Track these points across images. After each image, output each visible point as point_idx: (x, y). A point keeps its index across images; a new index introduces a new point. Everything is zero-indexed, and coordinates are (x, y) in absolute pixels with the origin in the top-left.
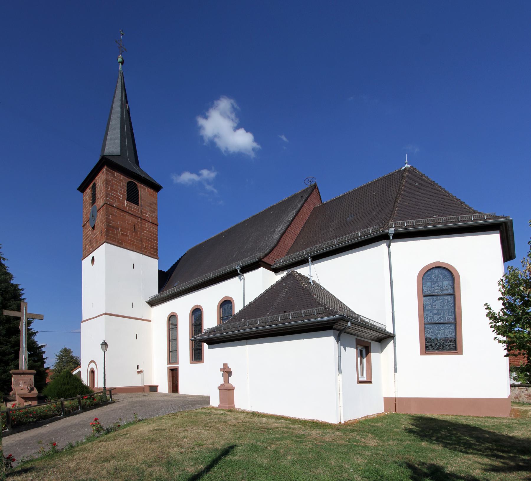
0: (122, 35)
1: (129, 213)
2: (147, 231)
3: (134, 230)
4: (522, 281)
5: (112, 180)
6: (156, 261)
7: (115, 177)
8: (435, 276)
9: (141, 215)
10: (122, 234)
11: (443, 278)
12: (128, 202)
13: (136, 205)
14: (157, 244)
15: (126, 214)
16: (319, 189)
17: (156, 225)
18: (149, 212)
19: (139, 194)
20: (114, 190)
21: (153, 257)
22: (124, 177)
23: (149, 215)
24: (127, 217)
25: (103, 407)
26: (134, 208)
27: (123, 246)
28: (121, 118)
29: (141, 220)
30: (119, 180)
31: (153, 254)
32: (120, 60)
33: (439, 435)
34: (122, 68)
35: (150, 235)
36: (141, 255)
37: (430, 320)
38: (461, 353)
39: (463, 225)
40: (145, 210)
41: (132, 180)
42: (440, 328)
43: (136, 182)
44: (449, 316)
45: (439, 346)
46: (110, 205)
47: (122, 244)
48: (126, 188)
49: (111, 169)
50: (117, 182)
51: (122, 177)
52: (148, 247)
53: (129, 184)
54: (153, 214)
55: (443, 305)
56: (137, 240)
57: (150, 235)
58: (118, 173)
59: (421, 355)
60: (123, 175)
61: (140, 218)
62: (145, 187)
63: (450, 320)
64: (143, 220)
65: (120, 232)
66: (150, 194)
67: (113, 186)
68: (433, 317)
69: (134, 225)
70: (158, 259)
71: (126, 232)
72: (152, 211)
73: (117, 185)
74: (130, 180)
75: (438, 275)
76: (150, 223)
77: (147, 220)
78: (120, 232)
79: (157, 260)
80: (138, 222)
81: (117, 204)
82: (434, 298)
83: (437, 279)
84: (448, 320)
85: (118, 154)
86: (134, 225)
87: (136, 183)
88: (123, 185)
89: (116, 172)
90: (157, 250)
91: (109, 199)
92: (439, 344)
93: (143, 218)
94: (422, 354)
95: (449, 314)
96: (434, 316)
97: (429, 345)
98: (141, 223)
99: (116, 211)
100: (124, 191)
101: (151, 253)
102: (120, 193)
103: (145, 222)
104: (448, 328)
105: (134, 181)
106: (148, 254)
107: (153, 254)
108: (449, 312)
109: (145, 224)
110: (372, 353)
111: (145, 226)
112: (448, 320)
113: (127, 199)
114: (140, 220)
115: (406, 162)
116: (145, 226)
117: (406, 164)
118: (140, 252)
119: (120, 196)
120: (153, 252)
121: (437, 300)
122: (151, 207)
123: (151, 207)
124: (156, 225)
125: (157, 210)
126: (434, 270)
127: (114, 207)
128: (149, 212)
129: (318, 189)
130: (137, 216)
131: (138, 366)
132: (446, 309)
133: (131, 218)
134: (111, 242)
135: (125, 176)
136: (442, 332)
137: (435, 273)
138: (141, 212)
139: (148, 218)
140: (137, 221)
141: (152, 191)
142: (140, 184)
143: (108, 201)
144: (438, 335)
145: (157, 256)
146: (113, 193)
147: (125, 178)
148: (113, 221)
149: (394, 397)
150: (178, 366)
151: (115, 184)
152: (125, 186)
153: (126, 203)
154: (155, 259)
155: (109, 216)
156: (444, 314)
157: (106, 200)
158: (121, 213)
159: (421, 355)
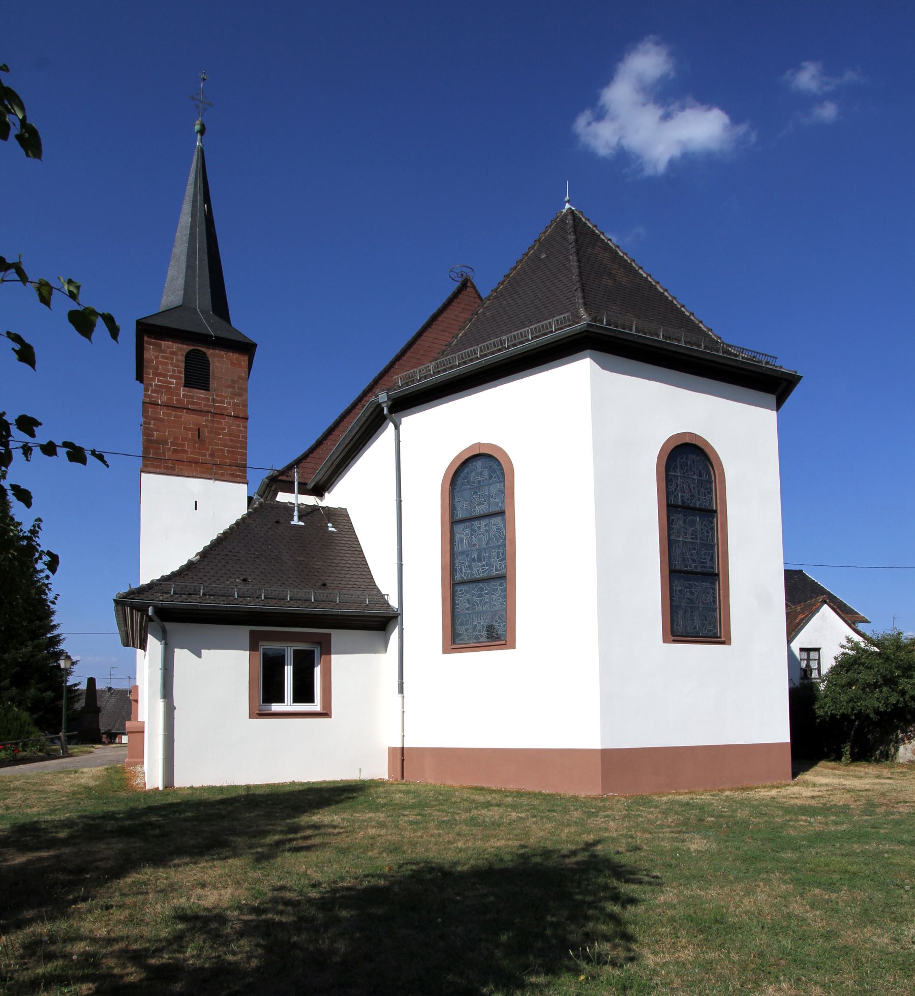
0: (204, 79)
1: (188, 409)
2: (225, 434)
3: (199, 438)
5: (157, 357)
7: (161, 351)
8: (477, 474)
9: (214, 406)
10: (175, 451)
11: (491, 477)
12: (187, 389)
13: (202, 391)
14: (245, 454)
15: (183, 412)
16: (477, 288)
17: (243, 418)
18: (228, 398)
19: (211, 368)
20: (160, 375)
21: (236, 481)
22: (180, 345)
23: (229, 403)
24: (185, 416)
26: (198, 398)
27: (174, 473)
28: (191, 234)
29: (213, 417)
30: (170, 354)
32: (197, 128)
33: (809, 819)
34: (201, 141)
35: (231, 441)
36: (212, 481)
37: (465, 575)
38: (513, 646)
39: (504, 356)
40: (221, 396)
41: (196, 348)
42: (483, 591)
43: (205, 348)
44: (499, 561)
45: (479, 631)
46: (152, 404)
47: (173, 468)
48: (183, 365)
49: (154, 339)
50: (167, 358)
51: (175, 346)
53: (189, 357)
54: (237, 400)
55: (489, 537)
56: (205, 455)
57: (231, 441)
58: (168, 341)
59: (664, 642)
60: (178, 343)
61: (211, 412)
62: (222, 353)
63: (500, 570)
64: (216, 416)
65: (170, 448)
66: (233, 363)
67: (157, 368)
68: (470, 568)
69: (199, 429)
70: (247, 484)
71: (183, 445)
72: (235, 395)
73: (166, 364)
74: (192, 348)
75: (481, 473)
76: (232, 418)
77: (224, 415)
78: (170, 448)
79: (246, 485)
80: (206, 420)
81: (165, 398)
82: (473, 525)
83: (479, 482)
84: (496, 570)
85: (178, 305)
86: (199, 429)
87: (204, 349)
88: (177, 360)
89: (164, 341)
91: (150, 393)
93: (215, 412)
94: (446, 651)
95: (498, 558)
96: (474, 564)
98: (212, 422)
99: (162, 412)
100: (180, 372)
101: (232, 475)
102: (172, 377)
103: (221, 418)
104: (497, 589)
105: (200, 348)
107: (237, 476)
108: (498, 553)
109: (220, 423)
111: (220, 426)
112: (496, 570)
113: (185, 383)
114: (211, 415)
115: (567, 198)
116: (220, 426)
117: (567, 204)
118: (209, 477)
119: (172, 383)
120: (236, 471)
121: (479, 528)
122: (234, 387)
124: (243, 418)
125: (246, 390)
126: (474, 463)
127: (159, 405)
128: (228, 398)
129: (474, 287)
130: (204, 411)
132: (494, 547)
133: (194, 417)
134: (152, 470)
135: (182, 343)
136: (486, 598)
137: (477, 468)
138: (213, 400)
139: (226, 408)
140: (202, 420)
141: (236, 356)
142: (211, 351)
143: (150, 396)
144: (478, 606)
145: (245, 477)
146: (159, 381)
147: (182, 346)
148: (156, 431)
149: (400, 746)
151: (162, 363)
152: (182, 362)
154: (241, 485)
155: (150, 424)
156: (490, 557)
157: (146, 396)
158: (174, 413)
159: (664, 642)
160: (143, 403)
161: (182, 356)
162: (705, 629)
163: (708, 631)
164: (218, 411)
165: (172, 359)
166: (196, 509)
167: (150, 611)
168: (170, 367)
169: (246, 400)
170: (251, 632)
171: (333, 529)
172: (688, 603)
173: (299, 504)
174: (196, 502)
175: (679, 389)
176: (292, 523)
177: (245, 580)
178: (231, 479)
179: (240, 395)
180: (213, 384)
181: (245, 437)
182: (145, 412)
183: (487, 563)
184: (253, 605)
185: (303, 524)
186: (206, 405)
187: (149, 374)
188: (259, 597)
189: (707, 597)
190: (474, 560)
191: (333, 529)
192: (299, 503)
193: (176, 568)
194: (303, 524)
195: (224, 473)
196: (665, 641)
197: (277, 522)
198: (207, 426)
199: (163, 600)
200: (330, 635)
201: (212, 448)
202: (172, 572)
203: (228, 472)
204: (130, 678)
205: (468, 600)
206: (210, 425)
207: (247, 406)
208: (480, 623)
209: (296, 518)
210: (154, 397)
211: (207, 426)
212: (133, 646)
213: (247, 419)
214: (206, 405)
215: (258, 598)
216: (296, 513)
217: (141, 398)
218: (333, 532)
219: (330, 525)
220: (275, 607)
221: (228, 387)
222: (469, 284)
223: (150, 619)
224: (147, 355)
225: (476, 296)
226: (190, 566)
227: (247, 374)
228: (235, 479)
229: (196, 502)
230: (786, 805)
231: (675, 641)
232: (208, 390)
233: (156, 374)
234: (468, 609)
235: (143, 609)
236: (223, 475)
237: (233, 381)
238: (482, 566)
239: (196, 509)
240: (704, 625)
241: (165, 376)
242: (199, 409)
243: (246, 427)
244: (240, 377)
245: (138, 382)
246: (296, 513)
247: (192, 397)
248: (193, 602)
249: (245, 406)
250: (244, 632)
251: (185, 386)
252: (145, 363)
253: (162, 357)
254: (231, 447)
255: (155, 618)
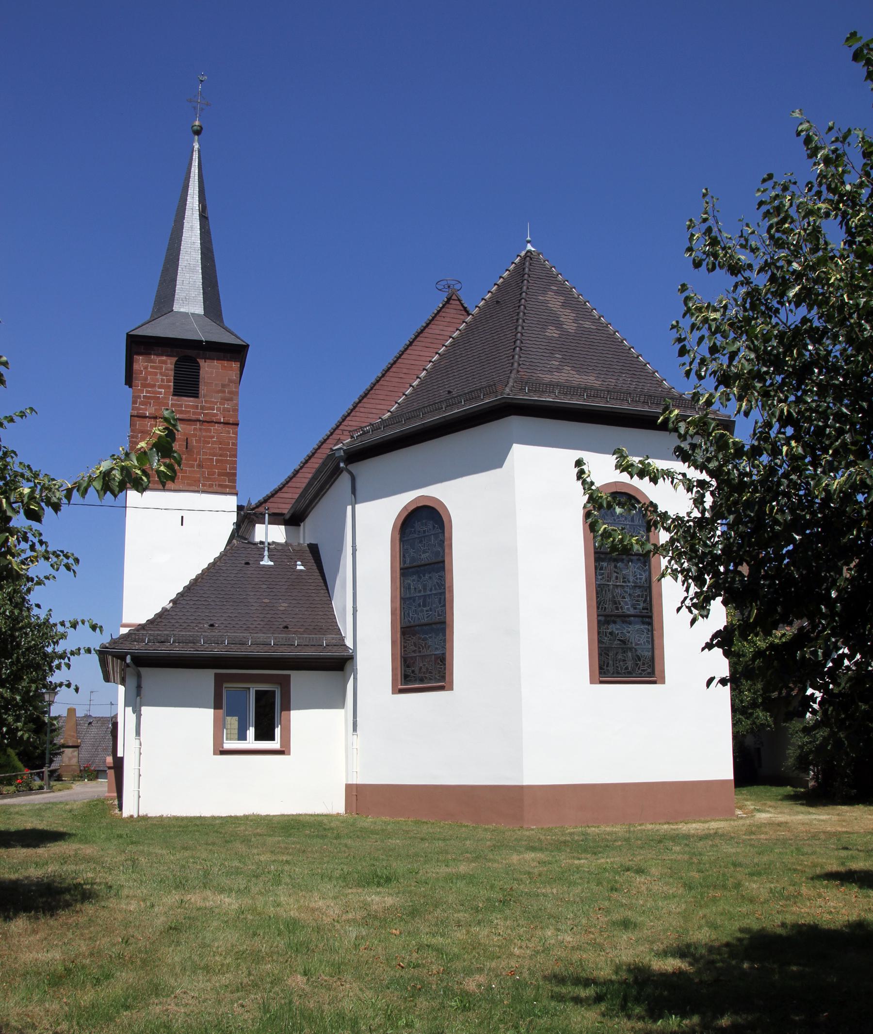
3: (187, 448)
4: (768, 383)
5: (146, 368)
6: (235, 498)
12: (176, 398)
13: (191, 399)
17: (233, 424)
23: (218, 409)
25: (769, 787)
26: (186, 406)
31: (226, 486)
48: (172, 373)
52: (214, 473)
56: (192, 466)
59: (591, 683)
67: (146, 379)
70: (237, 494)
73: (156, 374)
76: (222, 425)
80: (195, 429)
90: (235, 475)
92: (424, 670)
97: (409, 671)
98: (200, 429)
100: (169, 381)
101: (220, 486)
102: (160, 387)
106: (215, 488)
107: (226, 486)
109: (210, 431)
110: (292, 712)
112: (439, 615)
119: (160, 393)
122: (224, 392)
123: (224, 392)
124: (233, 424)
125: (237, 393)
138: (203, 408)
139: (216, 415)
145: (234, 487)
150: (274, 740)
151: (151, 373)
153: (171, 400)
159: (591, 683)
160: (131, 416)
161: (171, 364)
162: (639, 669)
163: (642, 670)
164: (208, 419)
165: (161, 368)
166: (182, 525)
167: (128, 659)
168: (159, 377)
169: (237, 405)
170: (216, 675)
171: (302, 568)
172: (620, 644)
173: (269, 544)
174: (182, 517)
175: (301, 711)
176: (262, 563)
177: (212, 625)
178: (220, 490)
179: (231, 399)
180: (203, 390)
181: (235, 444)
182: (132, 425)
183: (430, 609)
184: (216, 650)
185: (272, 563)
186: (194, 413)
187: (138, 383)
188: (223, 642)
189: (641, 637)
190: (419, 605)
191: (302, 568)
192: (270, 540)
193: (151, 616)
194: (272, 563)
195: (213, 485)
196: (592, 682)
197: (247, 563)
198: (195, 435)
199: (138, 648)
200: (289, 676)
201: (200, 458)
202: (148, 621)
203: (217, 483)
204: (112, 704)
205: (415, 643)
206: (198, 433)
207: (237, 410)
208: (424, 665)
209: (266, 558)
210: (142, 409)
211: (195, 435)
212: (114, 682)
213: (237, 424)
214: (194, 413)
215: (222, 644)
216: (266, 553)
217: (129, 412)
218: (301, 571)
219: (299, 563)
220: (237, 651)
221: (218, 392)
222: (454, 297)
223: (128, 666)
224: (136, 367)
225: (462, 309)
226: (162, 615)
227: (239, 376)
228: (223, 490)
229: (182, 517)
230: (777, 822)
231: (602, 682)
232: (197, 397)
233: (144, 386)
234: (414, 651)
235: (122, 657)
236: (211, 486)
237: (223, 386)
238: (427, 611)
239: (182, 525)
240: (637, 665)
241: (154, 386)
242: (188, 418)
243: (236, 434)
244: (231, 381)
245: (127, 386)
246: (266, 553)
247: (181, 406)
248: (163, 650)
249: (236, 410)
250: (206, 678)
251: (174, 395)
252: (134, 375)
253: (151, 367)
254: (220, 456)
255: (132, 665)
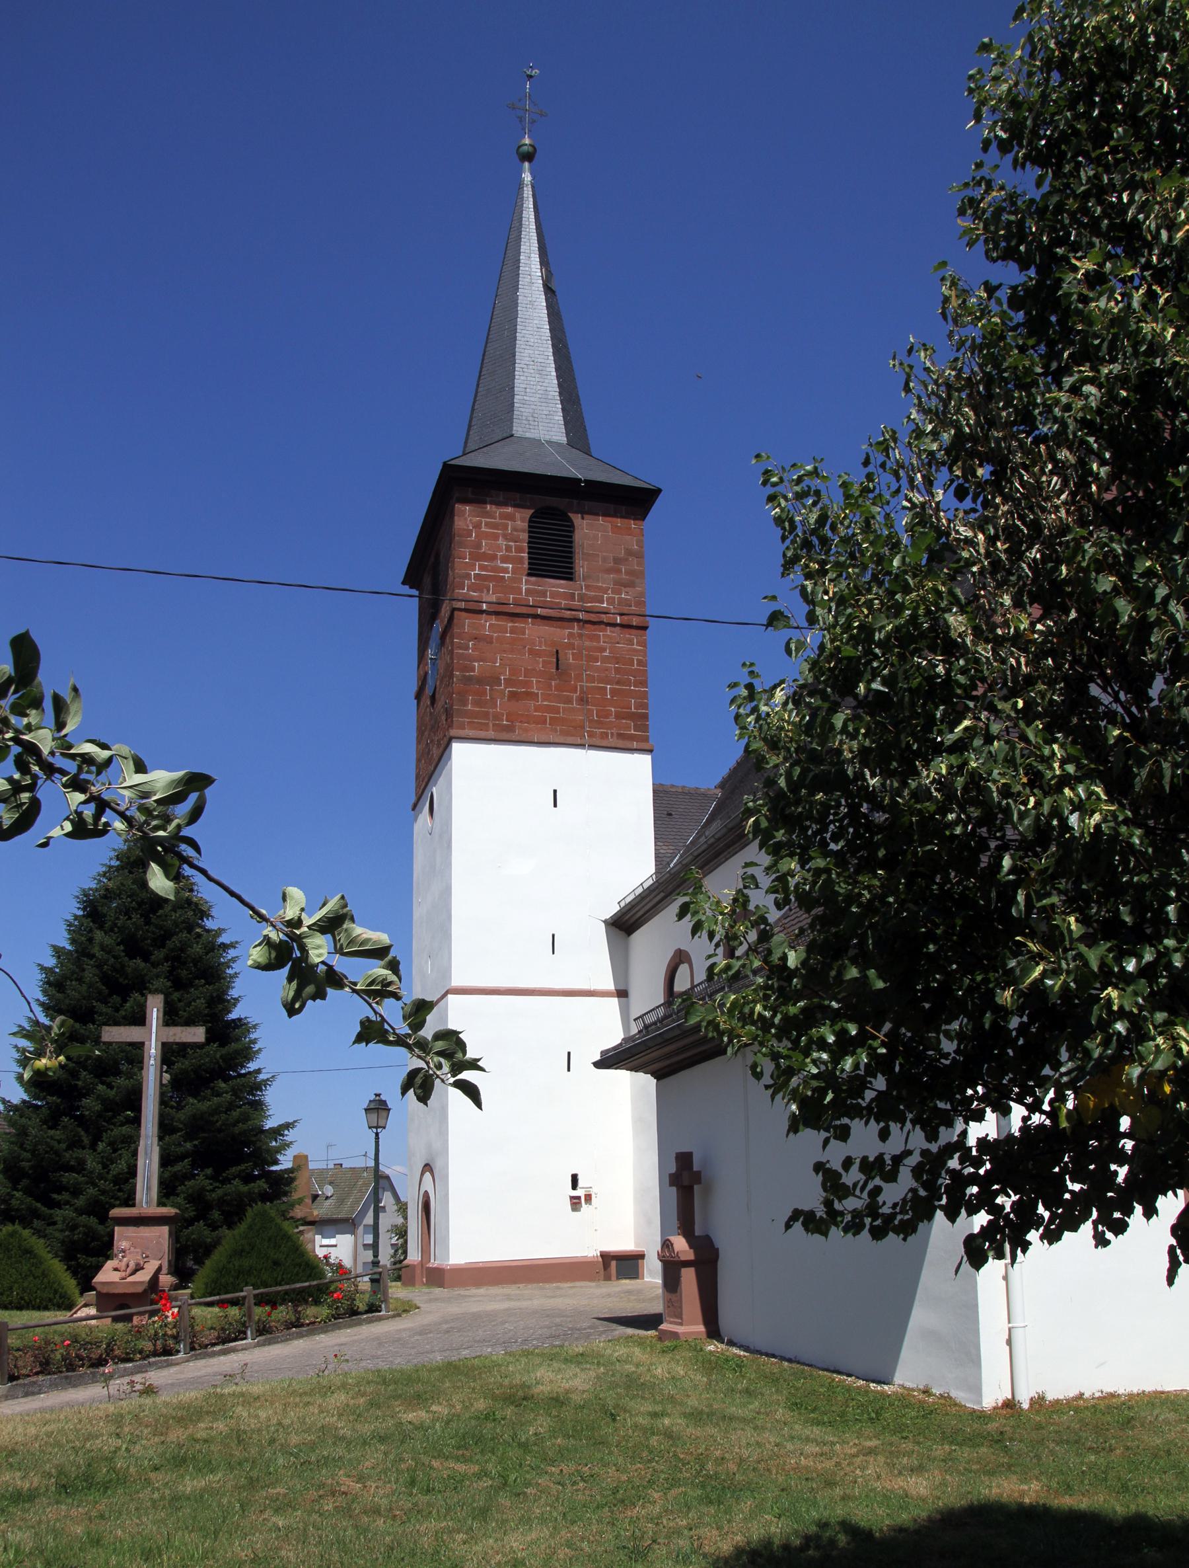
100: (519, 550)
131: (575, 1180)
243: (643, 644)
